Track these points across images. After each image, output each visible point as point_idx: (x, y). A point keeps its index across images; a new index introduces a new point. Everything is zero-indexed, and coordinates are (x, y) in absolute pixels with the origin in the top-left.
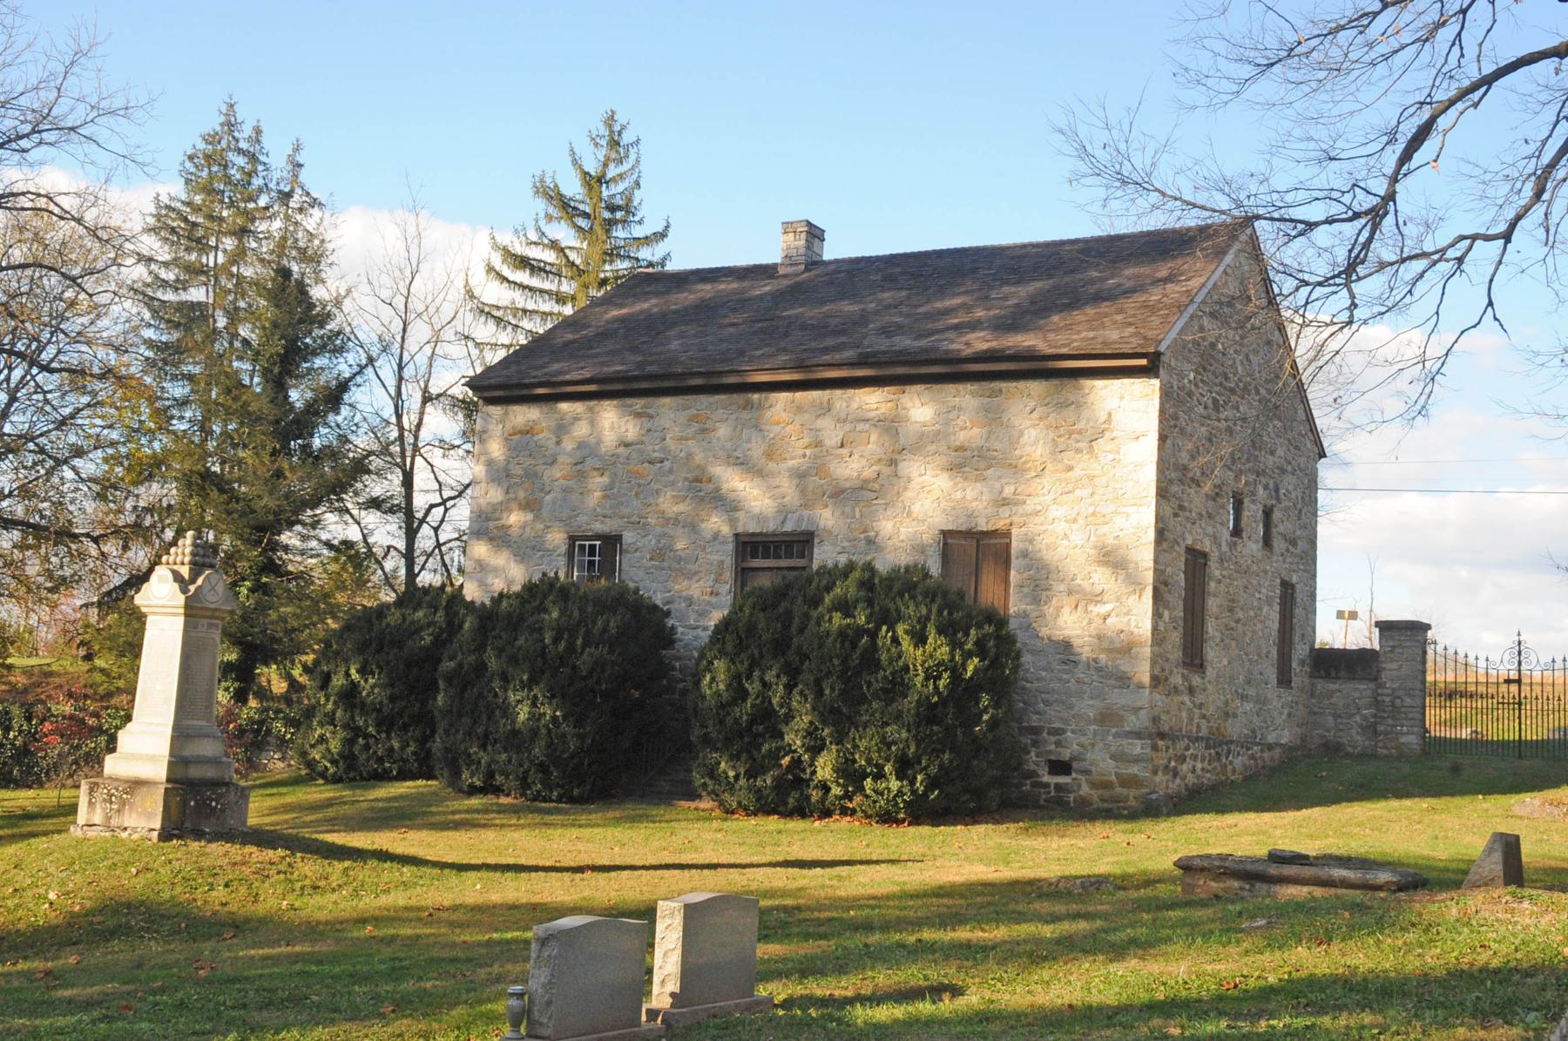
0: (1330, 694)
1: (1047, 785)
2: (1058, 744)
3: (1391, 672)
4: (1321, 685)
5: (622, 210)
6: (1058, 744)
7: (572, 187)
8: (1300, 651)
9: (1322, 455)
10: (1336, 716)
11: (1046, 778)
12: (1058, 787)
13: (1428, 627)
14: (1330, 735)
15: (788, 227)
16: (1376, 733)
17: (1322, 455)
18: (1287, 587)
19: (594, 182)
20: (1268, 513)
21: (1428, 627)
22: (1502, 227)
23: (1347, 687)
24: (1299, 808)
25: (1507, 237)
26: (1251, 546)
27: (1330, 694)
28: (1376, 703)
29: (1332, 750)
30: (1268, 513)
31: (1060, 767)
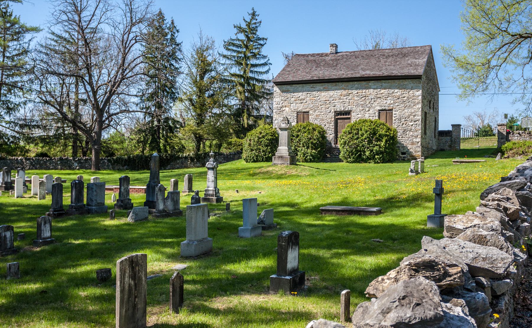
0: (442, 139)
1: (401, 157)
2: (403, 149)
3: (454, 134)
4: (440, 138)
5: (253, 30)
6: (403, 149)
7: (244, 25)
8: (437, 132)
9: (440, 91)
10: (443, 144)
11: (401, 156)
12: (403, 157)
13: (461, 125)
14: (442, 148)
15: (332, 45)
16: (451, 147)
17: (440, 91)
18: (435, 118)
19: (249, 25)
20: (433, 103)
21: (461, 125)
22: (500, 65)
23: (445, 138)
24: (446, 158)
25: (500, 66)
26: (432, 110)
27: (442, 139)
28: (451, 141)
29: (442, 150)
30: (433, 103)
31: (403, 153)
